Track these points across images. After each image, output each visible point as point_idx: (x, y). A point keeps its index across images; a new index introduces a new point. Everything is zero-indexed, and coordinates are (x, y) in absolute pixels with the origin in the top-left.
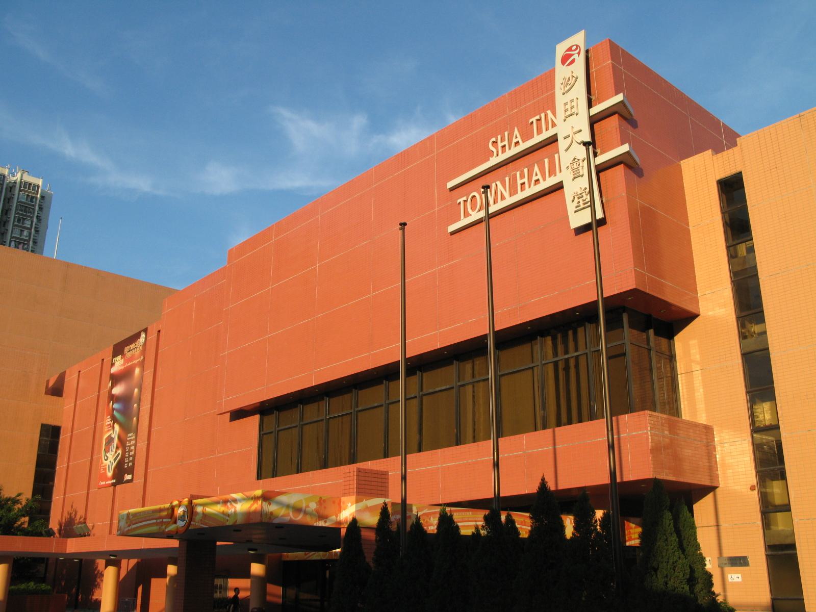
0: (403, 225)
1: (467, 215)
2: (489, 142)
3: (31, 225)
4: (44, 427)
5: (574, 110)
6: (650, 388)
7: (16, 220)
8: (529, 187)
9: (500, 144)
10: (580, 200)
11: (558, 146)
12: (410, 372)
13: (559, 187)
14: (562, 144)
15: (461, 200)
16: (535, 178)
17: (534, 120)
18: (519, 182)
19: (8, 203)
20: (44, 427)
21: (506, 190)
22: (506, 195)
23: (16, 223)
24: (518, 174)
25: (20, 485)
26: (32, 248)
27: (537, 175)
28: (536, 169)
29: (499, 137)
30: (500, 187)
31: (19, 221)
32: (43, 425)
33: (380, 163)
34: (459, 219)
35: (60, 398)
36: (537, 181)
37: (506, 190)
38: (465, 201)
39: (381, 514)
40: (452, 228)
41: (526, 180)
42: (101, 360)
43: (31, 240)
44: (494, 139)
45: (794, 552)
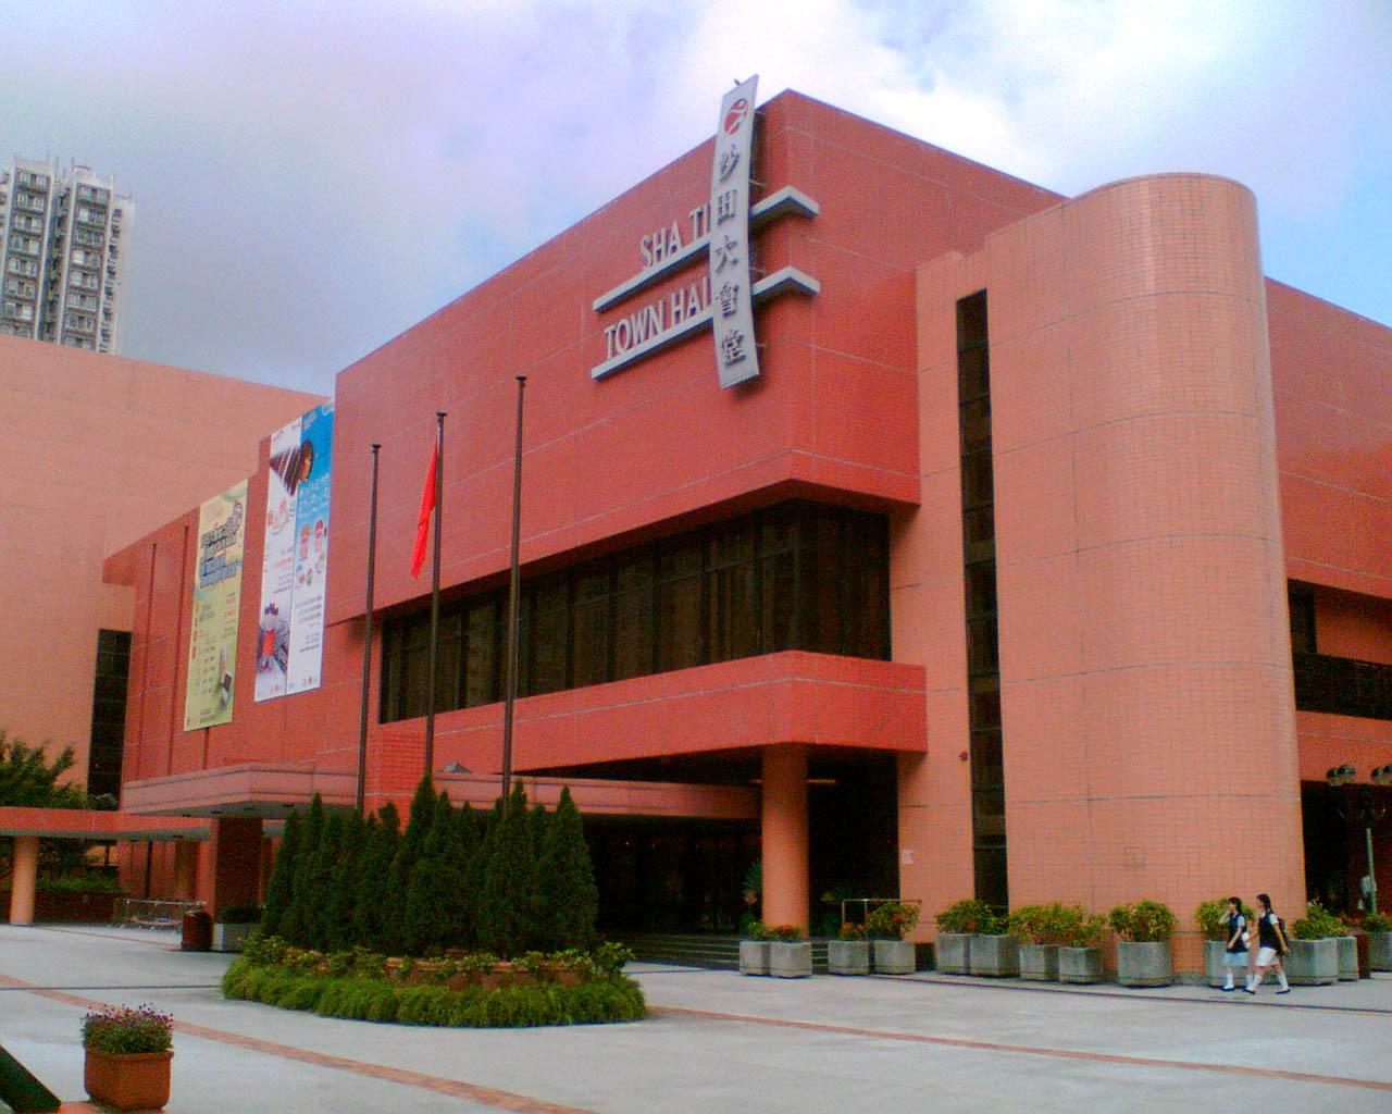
0: (522, 379)
1: (615, 353)
2: (640, 240)
3: (40, 251)
4: (105, 635)
5: (731, 211)
6: (866, 633)
7: (68, 321)
8: (685, 318)
9: (655, 249)
10: (730, 349)
11: (749, 228)
12: (445, 613)
13: (705, 330)
14: (715, 261)
15: (608, 330)
16: (691, 306)
17: (694, 212)
18: (674, 309)
19: (48, 331)
20: (105, 635)
21: (658, 315)
22: (659, 327)
23: (67, 326)
24: (673, 296)
25: (59, 727)
26: (101, 345)
27: (693, 301)
28: (693, 291)
29: (655, 236)
30: (652, 312)
31: (72, 321)
32: (102, 632)
33: (101, 1014)
34: (605, 360)
35: (896, 943)
36: (693, 311)
37: (658, 315)
38: (614, 332)
39: (420, 789)
40: (597, 371)
41: (681, 307)
42: (183, 529)
43: (99, 331)
44: (646, 238)
45: (1001, 847)
